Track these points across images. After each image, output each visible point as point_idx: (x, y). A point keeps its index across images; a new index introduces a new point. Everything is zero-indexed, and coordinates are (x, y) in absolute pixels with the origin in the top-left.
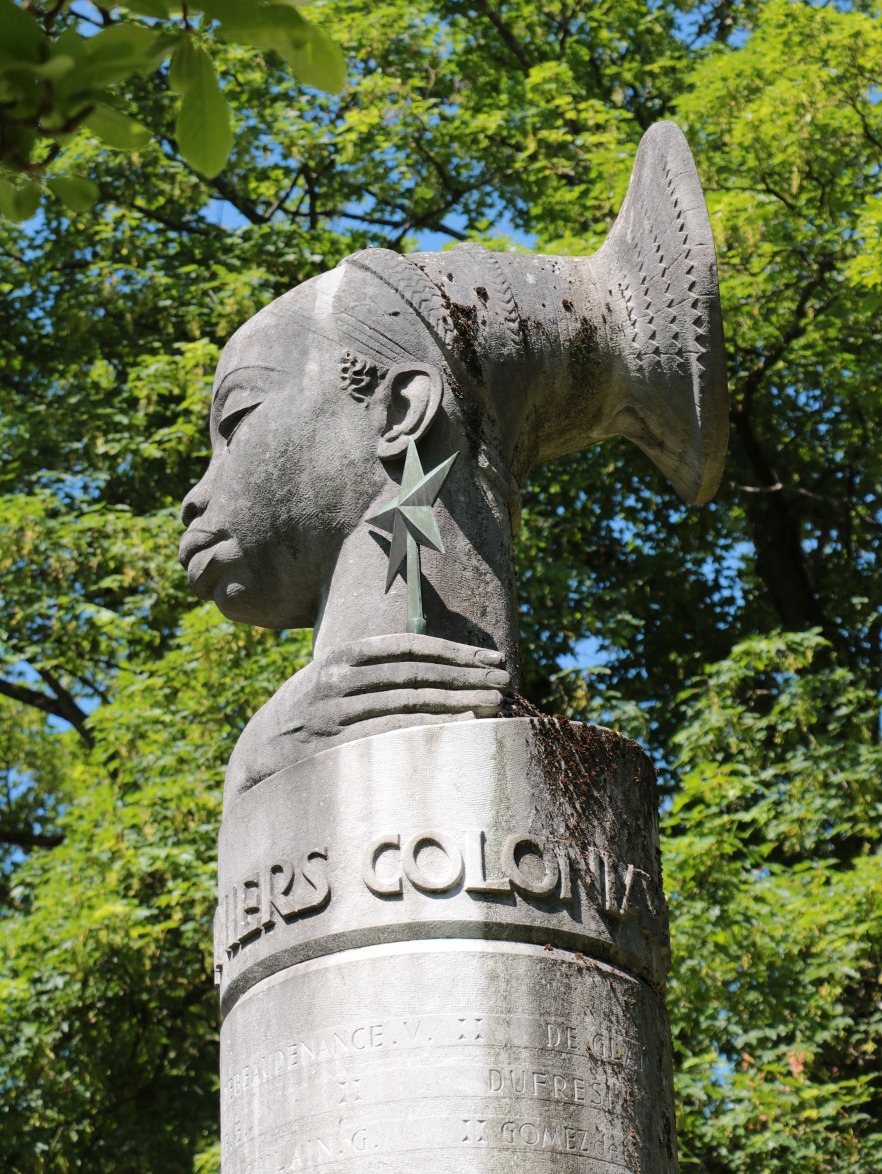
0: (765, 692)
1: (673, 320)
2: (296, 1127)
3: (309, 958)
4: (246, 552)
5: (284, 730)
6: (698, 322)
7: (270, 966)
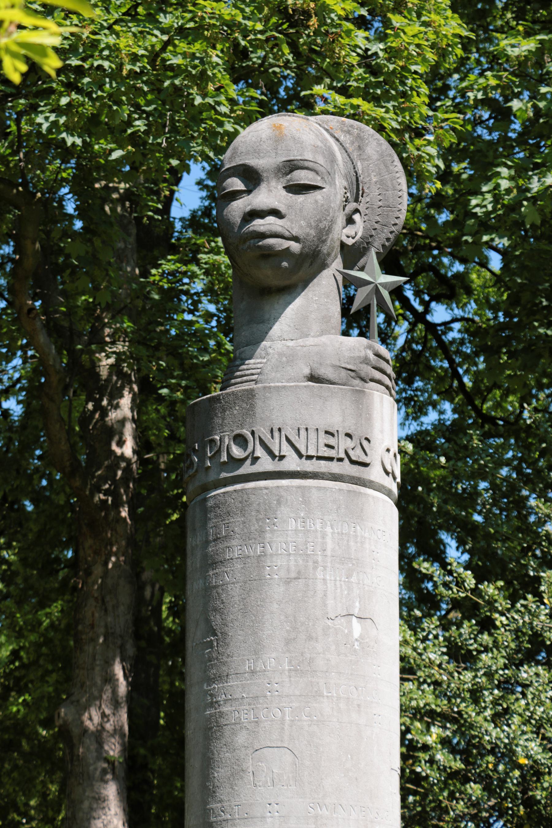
0: (163, 328)
1: (375, 229)
2: (354, 562)
3: (356, 484)
4: (301, 254)
5: (343, 365)
6: (388, 239)
7: (335, 478)
